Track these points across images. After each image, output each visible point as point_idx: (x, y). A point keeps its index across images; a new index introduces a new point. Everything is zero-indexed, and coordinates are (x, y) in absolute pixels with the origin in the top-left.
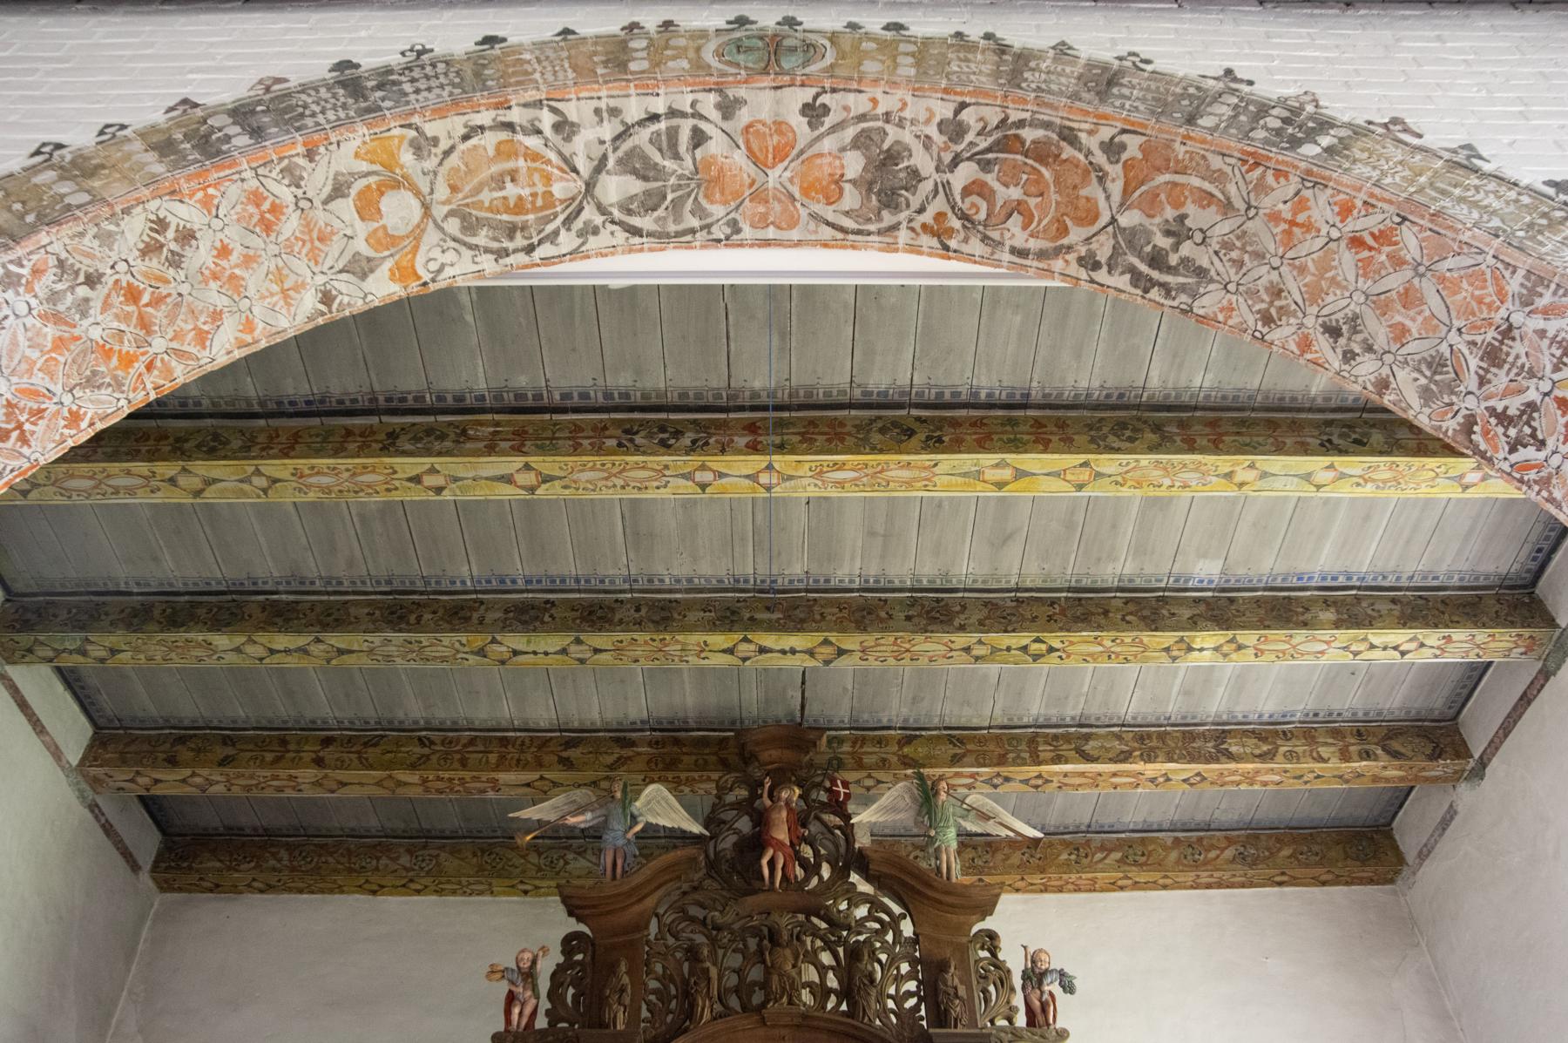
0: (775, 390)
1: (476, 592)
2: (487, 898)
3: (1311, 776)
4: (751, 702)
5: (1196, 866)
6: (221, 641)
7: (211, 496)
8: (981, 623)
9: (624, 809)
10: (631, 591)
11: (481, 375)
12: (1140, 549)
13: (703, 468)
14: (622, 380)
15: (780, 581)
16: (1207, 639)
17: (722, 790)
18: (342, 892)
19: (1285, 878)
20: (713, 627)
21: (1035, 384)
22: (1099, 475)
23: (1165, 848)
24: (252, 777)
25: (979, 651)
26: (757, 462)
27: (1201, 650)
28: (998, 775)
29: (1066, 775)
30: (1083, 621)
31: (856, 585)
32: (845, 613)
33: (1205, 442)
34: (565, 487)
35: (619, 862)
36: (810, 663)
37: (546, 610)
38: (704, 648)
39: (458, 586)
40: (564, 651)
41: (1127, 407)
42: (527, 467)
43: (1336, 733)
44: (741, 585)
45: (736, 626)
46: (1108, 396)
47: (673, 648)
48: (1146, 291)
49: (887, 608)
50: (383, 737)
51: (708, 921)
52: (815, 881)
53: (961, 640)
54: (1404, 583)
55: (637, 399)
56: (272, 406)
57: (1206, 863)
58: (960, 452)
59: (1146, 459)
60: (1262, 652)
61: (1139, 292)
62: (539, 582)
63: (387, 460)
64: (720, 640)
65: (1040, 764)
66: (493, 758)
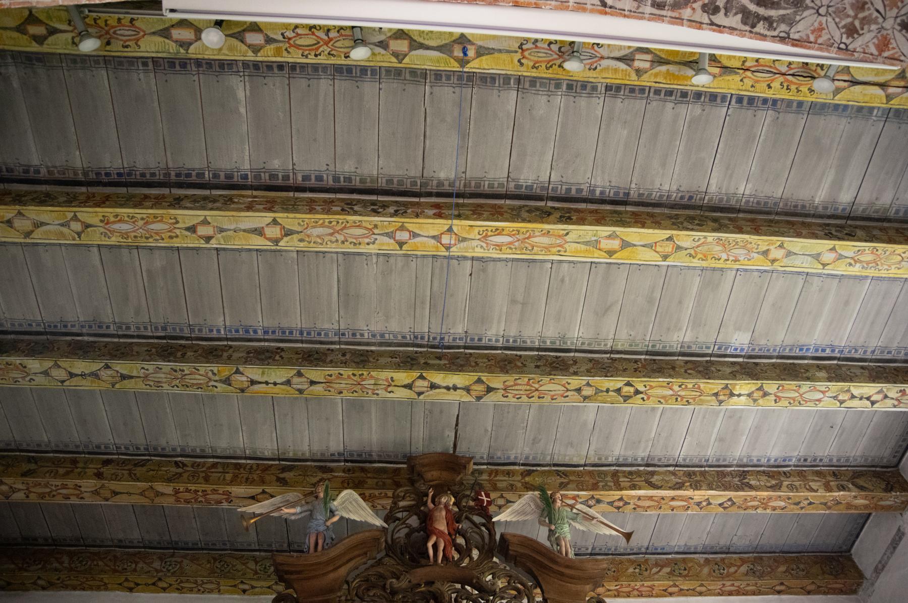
0: (454, 182)
1: (227, 339)
2: (215, 596)
3: (806, 502)
4: (420, 438)
5: (722, 577)
6: (34, 365)
7: (38, 236)
8: (588, 371)
9: (325, 503)
10: (340, 343)
11: (247, 158)
12: (697, 322)
13: (402, 228)
14: (347, 167)
15: (446, 338)
16: (744, 386)
17: (396, 499)
18: (106, 589)
19: (782, 588)
20: (398, 367)
21: (633, 186)
22: (679, 248)
23: (700, 566)
24: (46, 486)
25: (587, 392)
26: (442, 224)
27: (739, 395)
28: (593, 497)
29: (639, 499)
30: (659, 372)
31: (500, 344)
32: (493, 362)
33: (749, 229)
34: (301, 240)
35: (320, 542)
36: (467, 398)
37: (277, 353)
38: (390, 384)
39: (215, 334)
40: (288, 382)
41: (693, 207)
42: (275, 222)
43: (819, 474)
44: (419, 341)
45: (415, 367)
46: (682, 198)
47: (369, 382)
48: (753, 26)
49: (522, 360)
50: (149, 460)
51: (388, 586)
52: (467, 561)
53: (576, 382)
54: (869, 356)
55: (356, 183)
56: (92, 176)
57: (728, 575)
58: (584, 224)
59: (711, 236)
60: (780, 398)
61: (747, 28)
62: (274, 332)
63: (172, 212)
64: (403, 377)
65: (621, 489)
66: (229, 477)
